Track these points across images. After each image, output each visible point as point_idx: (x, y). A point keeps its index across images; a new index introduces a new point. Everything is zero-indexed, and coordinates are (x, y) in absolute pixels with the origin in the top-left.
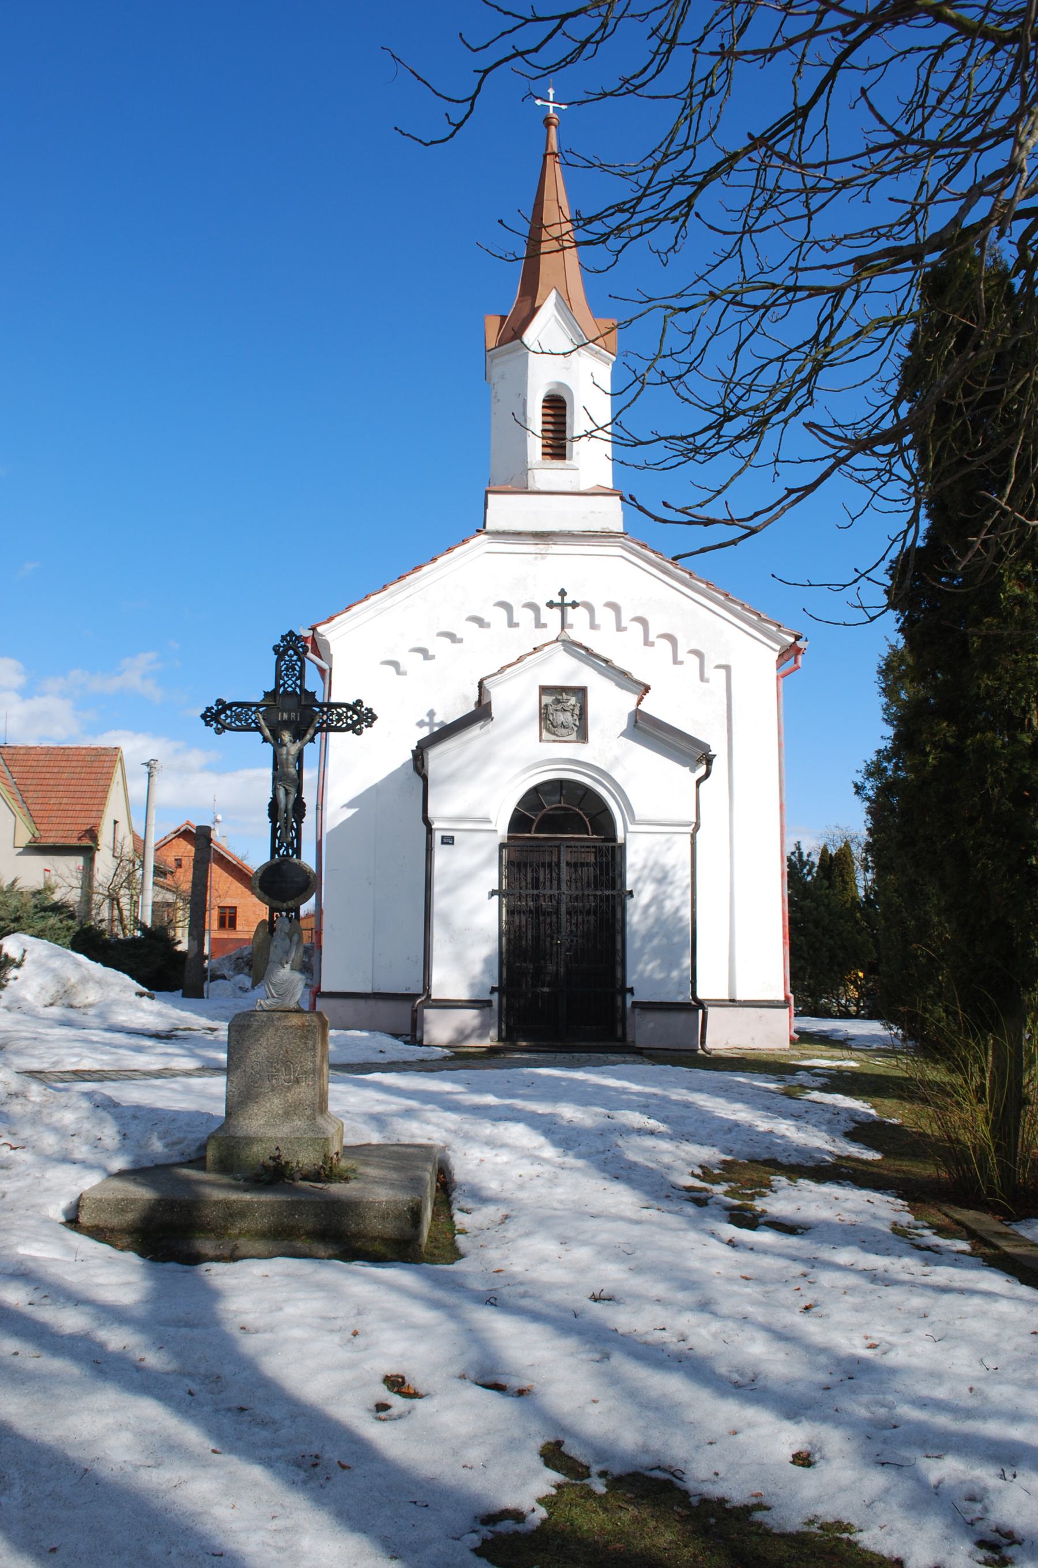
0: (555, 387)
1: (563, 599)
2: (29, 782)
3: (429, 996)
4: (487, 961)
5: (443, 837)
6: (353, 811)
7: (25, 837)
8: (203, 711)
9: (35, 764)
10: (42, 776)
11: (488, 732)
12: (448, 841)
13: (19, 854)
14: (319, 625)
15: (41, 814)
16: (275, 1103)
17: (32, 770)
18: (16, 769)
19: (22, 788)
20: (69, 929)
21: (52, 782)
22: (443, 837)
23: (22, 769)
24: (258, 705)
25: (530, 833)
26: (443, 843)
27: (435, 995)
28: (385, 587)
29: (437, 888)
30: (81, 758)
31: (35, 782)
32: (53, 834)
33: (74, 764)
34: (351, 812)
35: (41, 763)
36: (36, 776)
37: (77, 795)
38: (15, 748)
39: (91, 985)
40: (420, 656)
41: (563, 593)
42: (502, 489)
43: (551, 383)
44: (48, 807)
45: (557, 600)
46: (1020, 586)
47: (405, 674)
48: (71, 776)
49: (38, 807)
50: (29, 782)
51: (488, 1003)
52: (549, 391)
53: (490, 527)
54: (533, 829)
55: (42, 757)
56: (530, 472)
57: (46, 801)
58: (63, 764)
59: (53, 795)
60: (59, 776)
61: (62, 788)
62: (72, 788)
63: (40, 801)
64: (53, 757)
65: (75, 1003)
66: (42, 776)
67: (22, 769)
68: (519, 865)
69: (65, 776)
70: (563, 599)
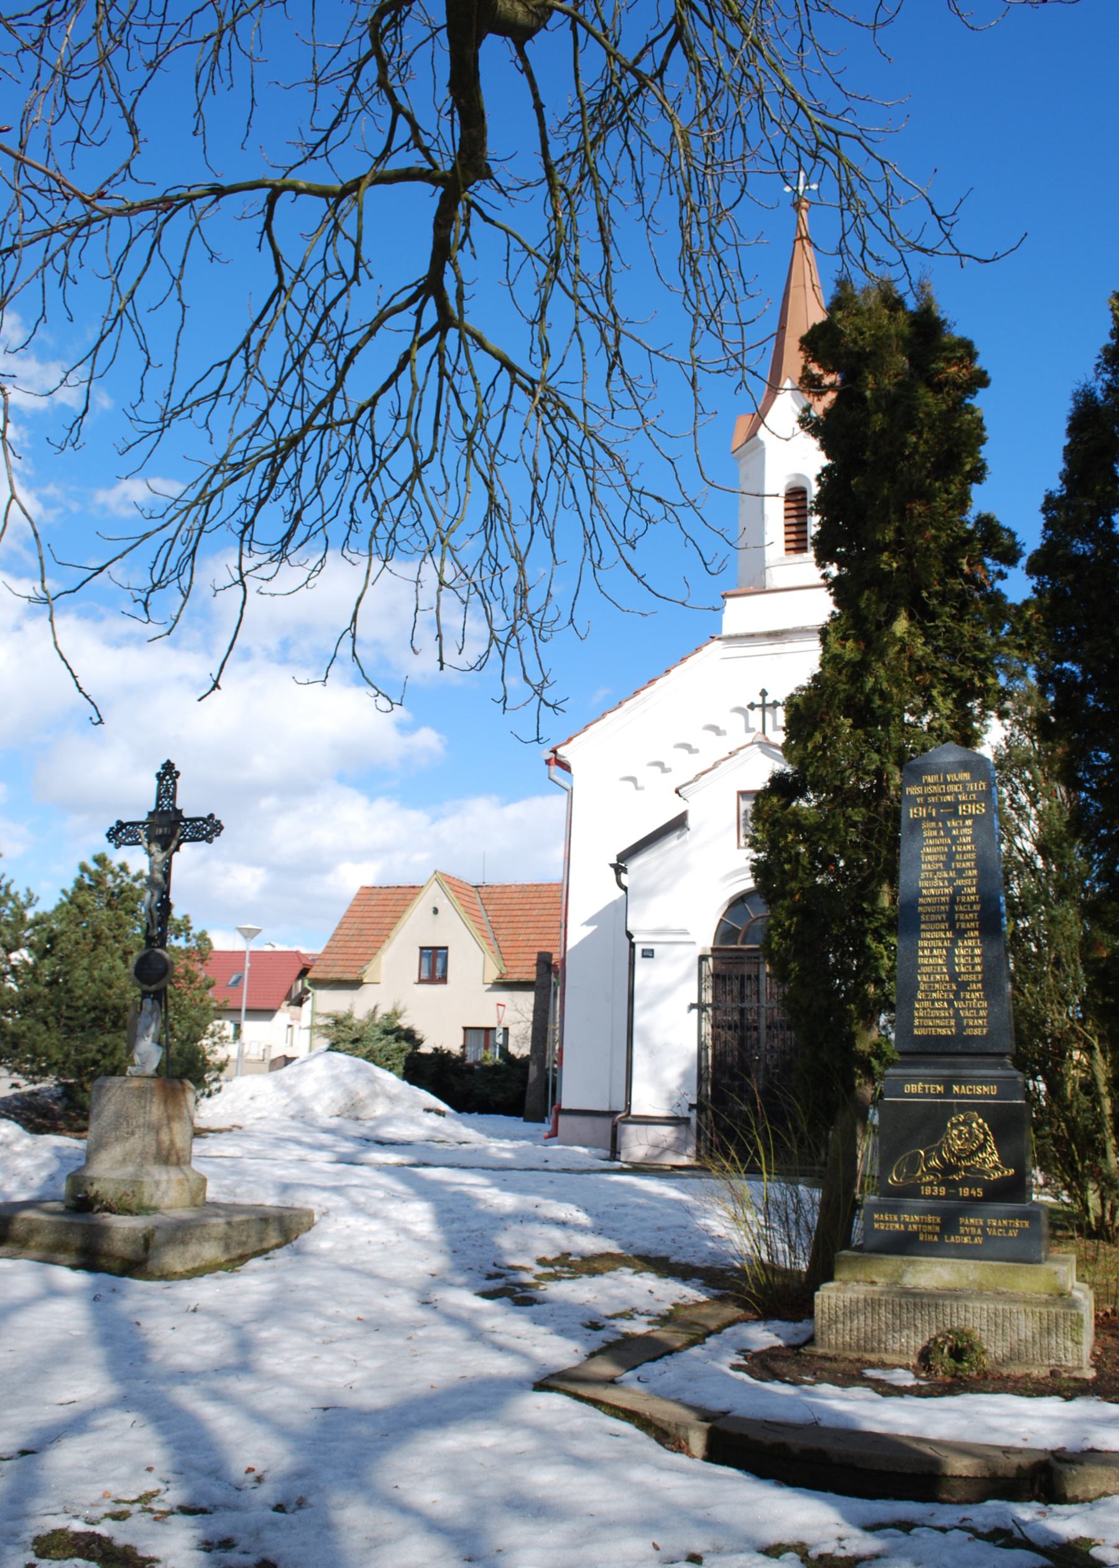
0: (793, 479)
1: (764, 700)
2: (501, 919)
3: (629, 1114)
4: (685, 1075)
5: (643, 951)
6: (594, 928)
7: (493, 974)
8: (107, 830)
9: (508, 901)
10: (515, 913)
11: (685, 842)
12: (648, 954)
13: (489, 990)
14: (559, 746)
15: (509, 950)
16: (116, 1151)
17: (506, 907)
18: (491, 907)
19: (495, 925)
20: (402, 1050)
21: (522, 919)
22: (643, 951)
23: (497, 907)
24: (144, 823)
25: (736, 943)
26: (643, 956)
27: (635, 1111)
28: (620, 704)
29: (637, 1004)
30: (551, 894)
31: (507, 919)
32: (518, 970)
33: (545, 900)
34: (593, 928)
35: (514, 901)
36: (509, 913)
37: (545, 930)
38: (492, 887)
39: (381, 1100)
40: (658, 769)
41: (764, 693)
42: (743, 590)
43: (789, 476)
44: (517, 944)
45: (758, 700)
46: (980, 648)
47: (642, 788)
48: (542, 912)
49: (507, 944)
50: (501, 919)
51: (687, 1121)
52: (789, 484)
53: (727, 630)
54: (740, 939)
55: (516, 895)
56: (767, 571)
57: (515, 937)
58: (535, 900)
59: (522, 931)
60: (530, 912)
61: (531, 925)
62: (540, 924)
63: (510, 938)
64: (526, 895)
65: (361, 1115)
66: (515, 913)
67: (497, 907)
68: (724, 978)
69: (535, 913)
70: (764, 700)
